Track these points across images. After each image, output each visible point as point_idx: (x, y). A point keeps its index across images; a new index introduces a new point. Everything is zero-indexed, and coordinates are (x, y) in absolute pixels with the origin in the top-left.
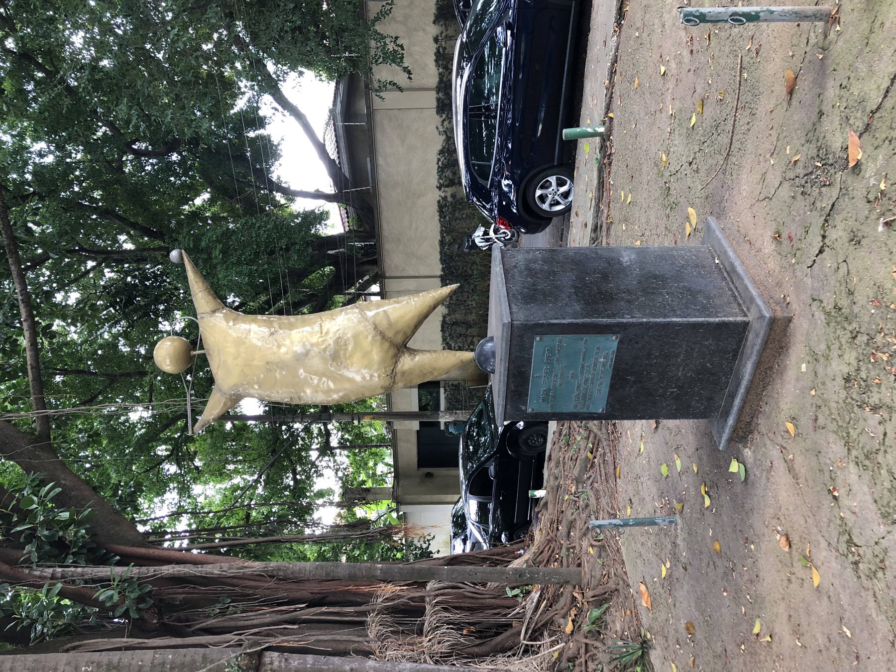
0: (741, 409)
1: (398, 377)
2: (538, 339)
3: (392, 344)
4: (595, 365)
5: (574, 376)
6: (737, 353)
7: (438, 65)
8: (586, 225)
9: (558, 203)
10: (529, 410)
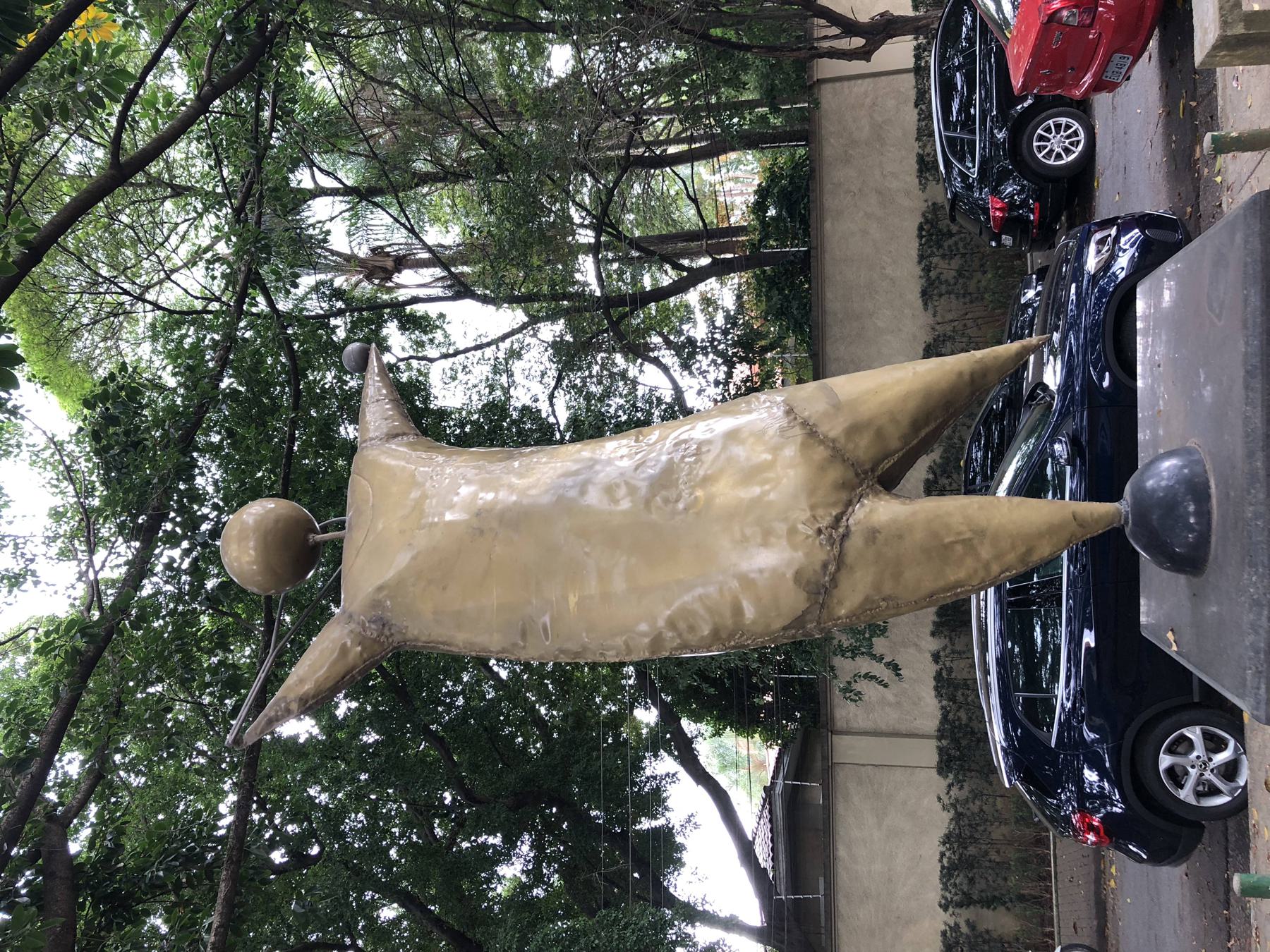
1: (855, 543)
3: (837, 454)
9: (1215, 791)
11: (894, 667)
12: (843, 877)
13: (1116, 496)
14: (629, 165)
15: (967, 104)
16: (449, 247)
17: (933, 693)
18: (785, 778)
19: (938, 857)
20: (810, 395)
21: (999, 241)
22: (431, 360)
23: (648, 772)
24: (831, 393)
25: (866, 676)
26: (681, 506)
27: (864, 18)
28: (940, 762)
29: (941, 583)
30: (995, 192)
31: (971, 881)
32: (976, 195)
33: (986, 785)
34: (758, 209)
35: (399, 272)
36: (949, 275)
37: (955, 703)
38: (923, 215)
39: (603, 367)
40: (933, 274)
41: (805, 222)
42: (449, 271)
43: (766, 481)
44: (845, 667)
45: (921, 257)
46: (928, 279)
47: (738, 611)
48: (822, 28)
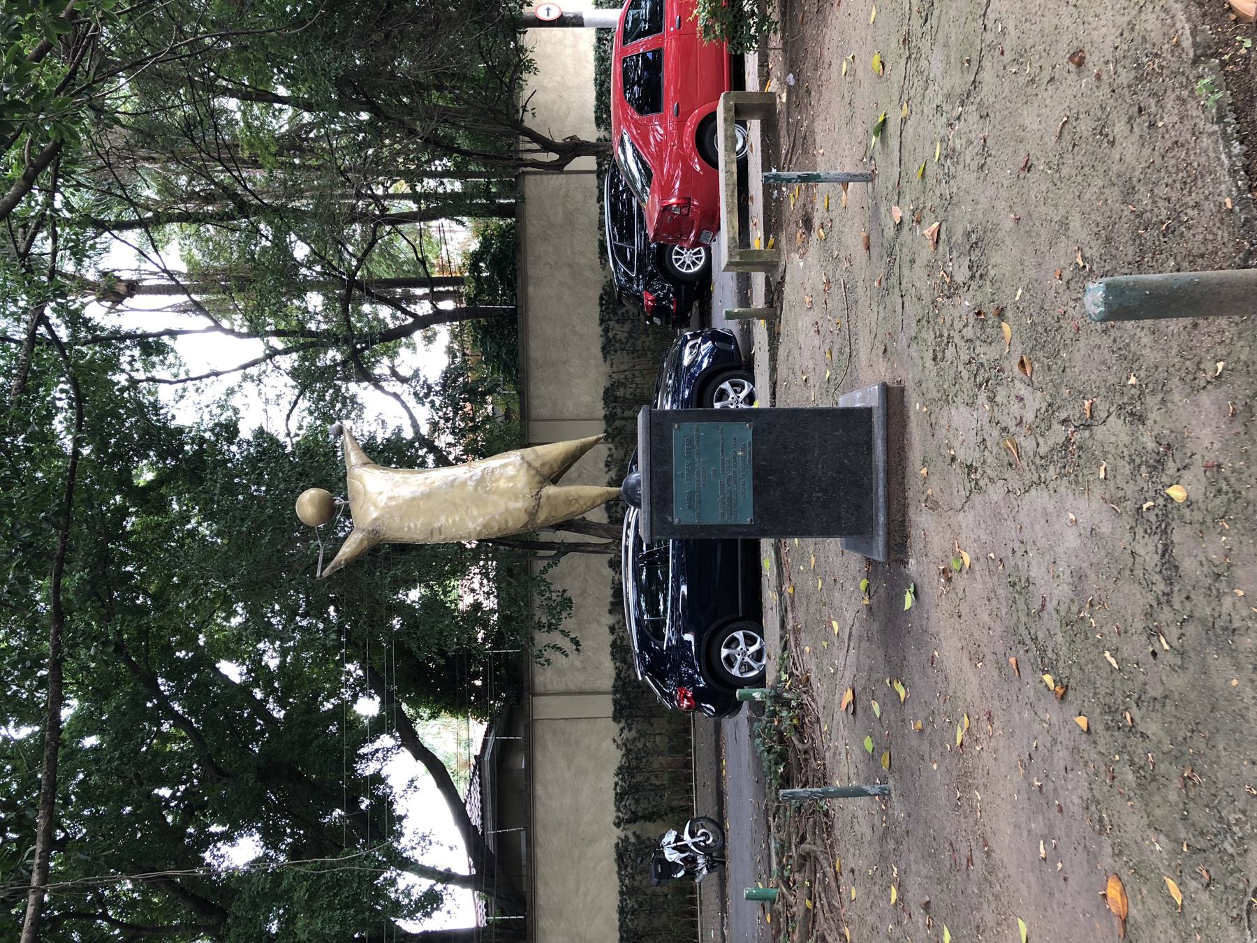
1: (543, 500)
3: (538, 473)
9: (752, 669)
11: (576, 642)
12: (541, 812)
13: (619, 486)
21: (652, 322)
24: (535, 451)
27: (558, 140)
31: (637, 801)
35: (132, 296)
36: (622, 336)
40: (610, 334)
44: (542, 638)
45: (602, 321)
46: (607, 338)
47: (507, 522)
48: (526, 144)
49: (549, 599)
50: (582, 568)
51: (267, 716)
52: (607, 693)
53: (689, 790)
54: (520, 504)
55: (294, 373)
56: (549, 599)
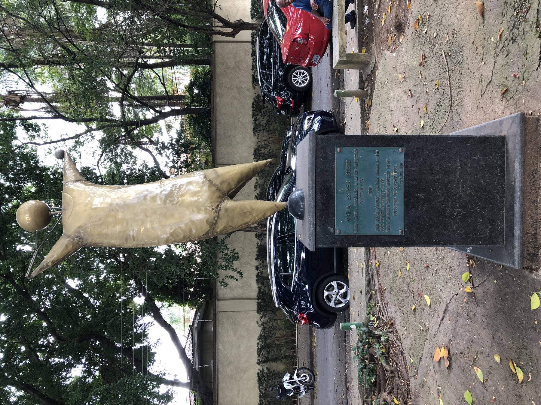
0: (523, 217)
1: (222, 212)
2: (338, 149)
3: (218, 189)
4: (389, 180)
5: (372, 191)
6: (503, 169)
7: (258, 282)
8: (361, 292)
9: (341, 303)
10: (337, 232)
11: (241, 273)
14: (136, 66)
15: (269, 57)
16: (49, 94)
17: (256, 282)
18: (198, 320)
19: (257, 345)
20: (210, 172)
21: (280, 113)
22: (39, 144)
23: (139, 323)
25: (230, 277)
26: (175, 202)
27: (232, 20)
28: (258, 308)
29: (244, 222)
30: (279, 94)
31: (268, 352)
32: (272, 95)
33: (274, 316)
34: (190, 88)
35: (23, 103)
36: (263, 123)
37: (263, 285)
38: (254, 99)
39: (122, 150)
40: (257, 122)
41: (209, 97)
42: (50, 105)
43: (199, 196)
44: (222, 273)
45: (253, 115)
46: (256, 124)
47: (191, 231)
48: (216, 23)
49: (227, 254)
50: (242, 237)
51: (91, 306)
52: (254, 299)
53: (294, 348)
54: (200, 216)
55: (102, 141)
56: (227, 254)
